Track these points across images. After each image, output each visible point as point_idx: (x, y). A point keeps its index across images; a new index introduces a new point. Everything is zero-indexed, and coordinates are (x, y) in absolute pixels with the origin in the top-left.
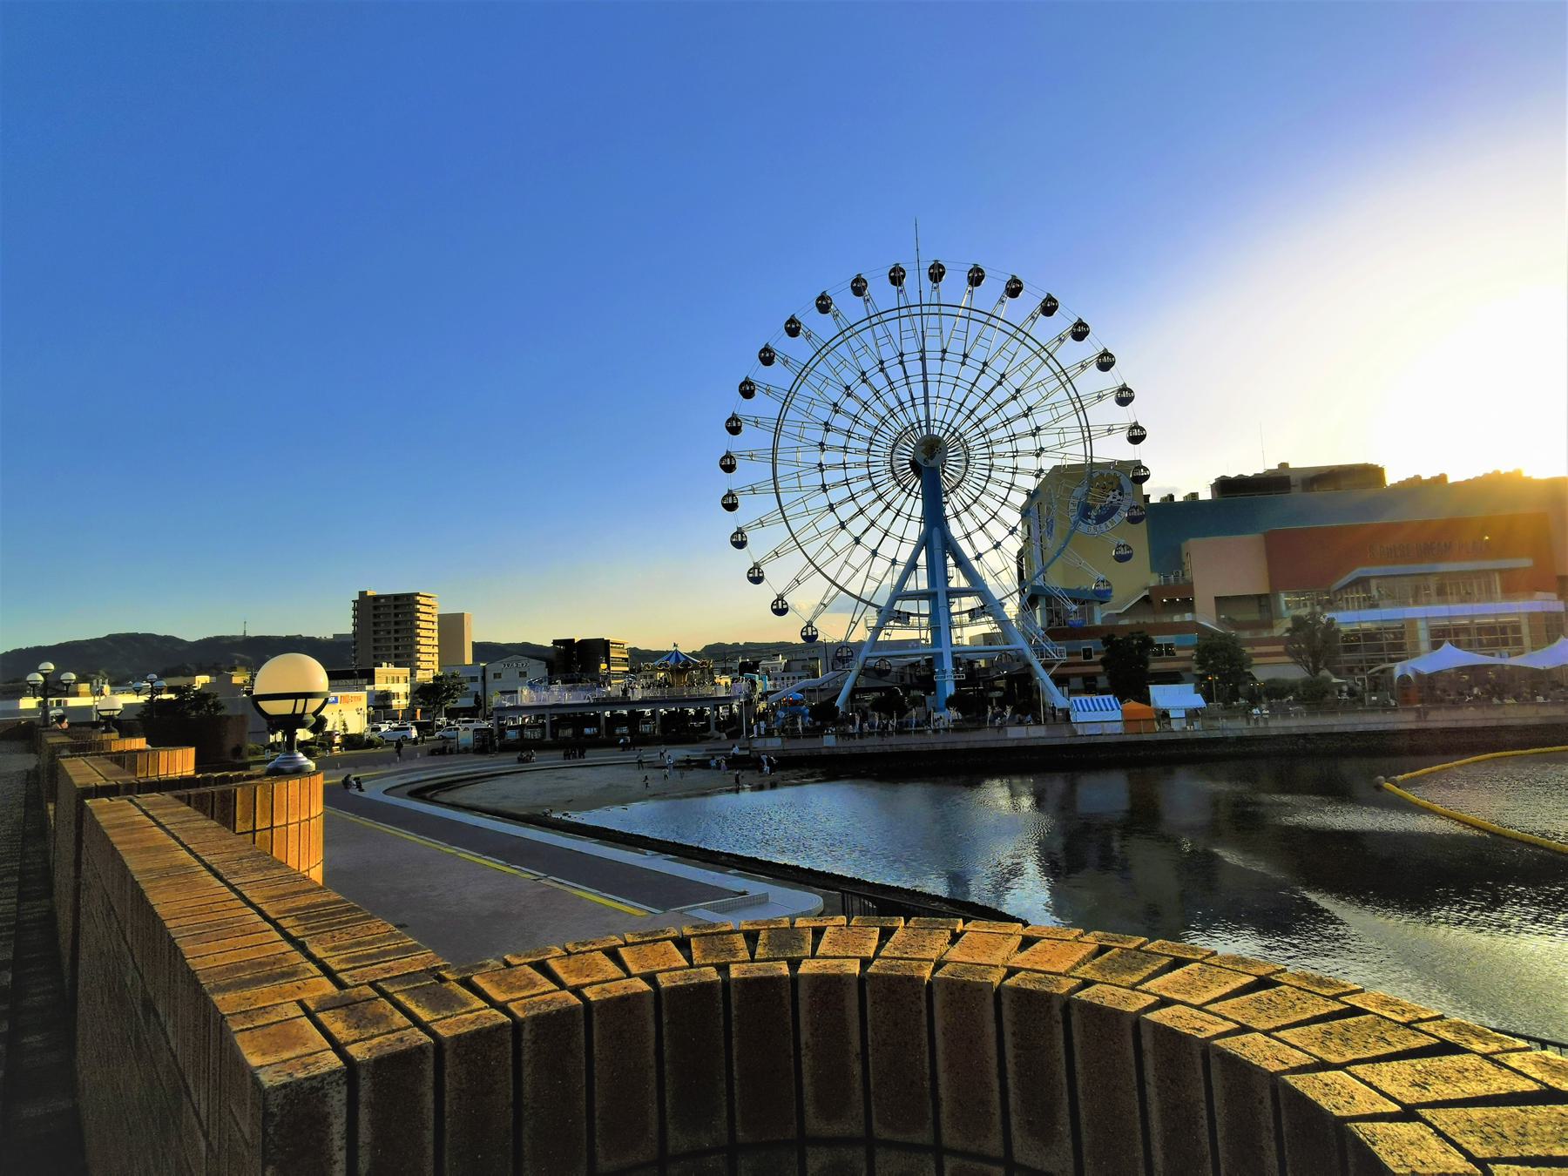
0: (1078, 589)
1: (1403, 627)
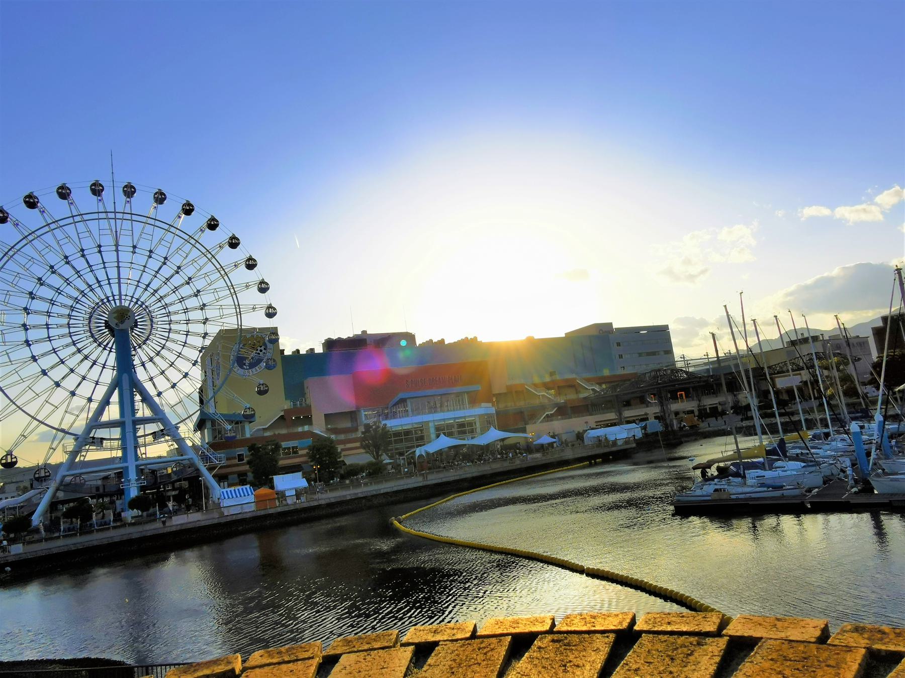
0: (234, 414)
1: (422, 427)
